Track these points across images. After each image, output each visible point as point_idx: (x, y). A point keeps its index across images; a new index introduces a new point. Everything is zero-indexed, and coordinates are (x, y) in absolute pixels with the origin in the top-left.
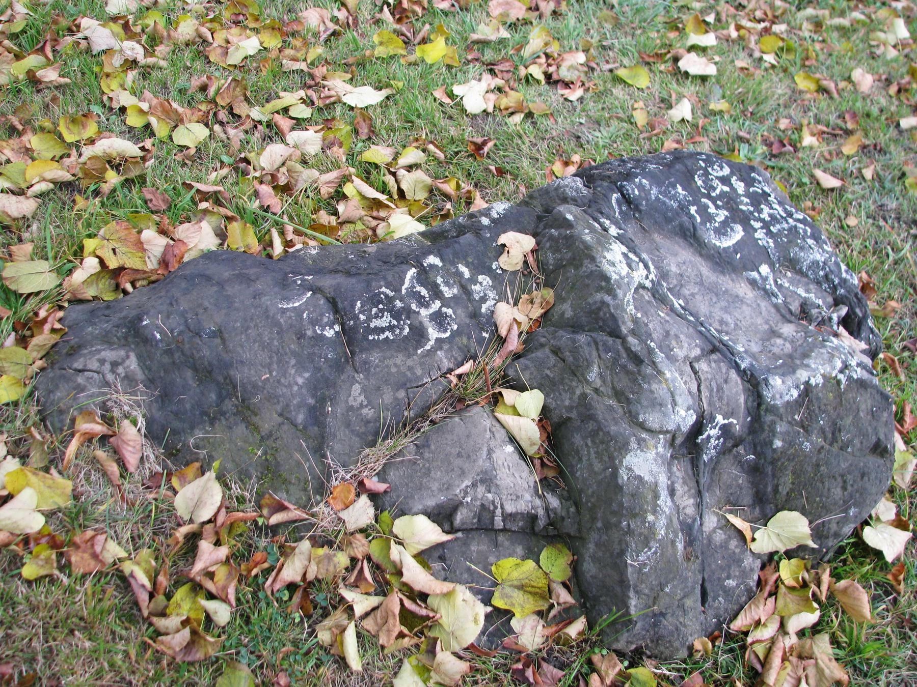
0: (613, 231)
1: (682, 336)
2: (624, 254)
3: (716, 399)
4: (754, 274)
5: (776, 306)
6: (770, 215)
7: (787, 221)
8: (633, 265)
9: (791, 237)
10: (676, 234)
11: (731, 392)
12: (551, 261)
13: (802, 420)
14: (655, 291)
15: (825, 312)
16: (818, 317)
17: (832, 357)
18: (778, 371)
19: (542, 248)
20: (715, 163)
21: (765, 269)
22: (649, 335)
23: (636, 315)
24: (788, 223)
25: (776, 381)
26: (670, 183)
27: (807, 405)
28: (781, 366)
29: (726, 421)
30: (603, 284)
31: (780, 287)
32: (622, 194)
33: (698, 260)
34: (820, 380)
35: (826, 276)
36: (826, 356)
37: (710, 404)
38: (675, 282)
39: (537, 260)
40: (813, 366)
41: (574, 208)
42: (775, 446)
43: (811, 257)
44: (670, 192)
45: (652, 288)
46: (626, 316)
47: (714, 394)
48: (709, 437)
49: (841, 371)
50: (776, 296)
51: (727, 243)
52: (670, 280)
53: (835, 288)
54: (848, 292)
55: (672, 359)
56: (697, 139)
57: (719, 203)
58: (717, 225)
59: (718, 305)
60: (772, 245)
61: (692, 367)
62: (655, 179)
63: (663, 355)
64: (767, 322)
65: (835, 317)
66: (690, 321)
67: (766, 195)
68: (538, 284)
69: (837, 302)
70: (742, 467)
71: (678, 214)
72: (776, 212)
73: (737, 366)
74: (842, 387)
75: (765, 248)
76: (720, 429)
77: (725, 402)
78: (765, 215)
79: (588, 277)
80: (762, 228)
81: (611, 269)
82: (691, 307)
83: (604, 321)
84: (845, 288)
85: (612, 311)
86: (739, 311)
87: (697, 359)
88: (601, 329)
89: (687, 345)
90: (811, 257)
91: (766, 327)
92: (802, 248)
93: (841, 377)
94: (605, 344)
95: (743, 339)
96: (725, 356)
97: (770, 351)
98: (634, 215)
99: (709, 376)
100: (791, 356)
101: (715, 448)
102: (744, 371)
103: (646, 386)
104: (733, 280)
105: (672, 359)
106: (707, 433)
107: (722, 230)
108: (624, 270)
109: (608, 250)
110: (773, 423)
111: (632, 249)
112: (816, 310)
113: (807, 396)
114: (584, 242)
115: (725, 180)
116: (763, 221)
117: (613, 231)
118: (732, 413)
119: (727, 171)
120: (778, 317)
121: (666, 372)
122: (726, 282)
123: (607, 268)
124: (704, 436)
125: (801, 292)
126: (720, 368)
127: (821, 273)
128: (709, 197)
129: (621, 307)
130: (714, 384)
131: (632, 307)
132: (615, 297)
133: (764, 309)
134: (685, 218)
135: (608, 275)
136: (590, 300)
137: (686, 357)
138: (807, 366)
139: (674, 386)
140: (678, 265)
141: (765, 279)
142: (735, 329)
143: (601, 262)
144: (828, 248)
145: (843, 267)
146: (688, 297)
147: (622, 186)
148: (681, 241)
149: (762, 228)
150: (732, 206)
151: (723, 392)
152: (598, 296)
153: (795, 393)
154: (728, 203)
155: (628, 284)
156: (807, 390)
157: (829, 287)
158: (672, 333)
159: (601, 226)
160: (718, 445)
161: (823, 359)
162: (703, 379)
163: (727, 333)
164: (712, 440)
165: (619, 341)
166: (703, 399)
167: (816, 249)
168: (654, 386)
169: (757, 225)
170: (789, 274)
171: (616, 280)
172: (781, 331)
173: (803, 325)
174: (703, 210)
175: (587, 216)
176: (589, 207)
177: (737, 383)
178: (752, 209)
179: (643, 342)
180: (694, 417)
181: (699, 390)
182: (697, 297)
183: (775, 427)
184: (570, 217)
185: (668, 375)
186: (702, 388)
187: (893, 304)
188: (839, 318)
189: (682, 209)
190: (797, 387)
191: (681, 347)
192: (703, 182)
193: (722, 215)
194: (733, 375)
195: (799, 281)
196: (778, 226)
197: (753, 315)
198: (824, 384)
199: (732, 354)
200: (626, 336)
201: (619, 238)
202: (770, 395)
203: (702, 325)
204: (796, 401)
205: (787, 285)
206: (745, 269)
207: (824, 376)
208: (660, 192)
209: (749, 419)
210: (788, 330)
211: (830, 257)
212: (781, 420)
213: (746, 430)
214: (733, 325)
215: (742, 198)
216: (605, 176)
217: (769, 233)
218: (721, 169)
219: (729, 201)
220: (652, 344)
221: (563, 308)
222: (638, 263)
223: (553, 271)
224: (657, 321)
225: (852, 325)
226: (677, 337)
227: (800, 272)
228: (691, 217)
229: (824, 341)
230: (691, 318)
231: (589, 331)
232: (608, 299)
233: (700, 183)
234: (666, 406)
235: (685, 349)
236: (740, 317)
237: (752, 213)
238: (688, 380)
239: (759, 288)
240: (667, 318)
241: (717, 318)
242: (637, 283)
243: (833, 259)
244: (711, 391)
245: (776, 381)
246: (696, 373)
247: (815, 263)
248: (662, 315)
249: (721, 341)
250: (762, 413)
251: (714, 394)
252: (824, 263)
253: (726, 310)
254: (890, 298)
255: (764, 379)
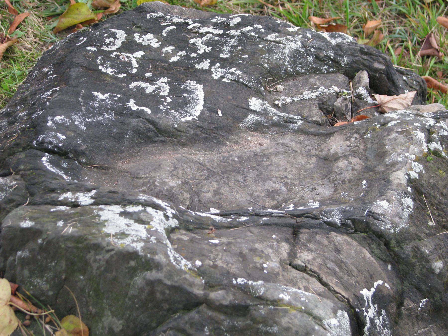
0: (85, 199)
1: (257, 245)
2: (121, 214)
3: (346, 277)
4: (251, 117)
5: (300, 131)
6: (207, 44)
7: (229, 35)
8: (143, 216)
9: (248, 48)
10: (139, 145)
11: (353, 257)
12: (45, 287)
13: (437, 222)
14: (186, 225)
15: (348, 94)
16: (346, 105)
17: (407, 133)
18: (373, 195)
19: (22, 281)
20: (101, 36)
21: (255, 103)
22: (229, 275)
23: (195, 266)
24: (232, 37)
25: (382, 206)
26: (83, 97)
27: (429, 202)
28: (369, 185)
29: (373, 290)
30: (133, 263)
31: (284, 108)
32: (50, 152)
33: (184, 152)
34: (419, 167)
35: (317, 57)
36: (402, 138)
37: (346, 288)
38: (187, 195)
39: (27, 299)
40: (400, 159)
41: (19, 211)
42: (437, 271)
43: (286, 51)
44: (94, 108)
45: (180, 224)
46: (187, 276)
47: (341, 274)
48: (372, 320)
49: (429, 140)
50: (292, 121)
51: (198, 109)
52: (181, 198)
53: (336, 62)
54: (352, 55)
55: (271, 277)
56: (19, 19)
57: (148, 75)
58: (169, 100)
59: (249, 181)
60: (239, 72)
61: (296, 267)
62: (69, 107)
63: (260, 282)
64: (310, 156)
65: (362, 90)
66: (245, 222)
67: (183, 26)
68: (50, 323)
69: (351, 74)
70: (423, 320)
71: (123, 123)
72: (210, 36)
73: (332, 226)
74: (443, 154)
75: (235, 81)
76: (374, 303)
77: (356, 273)
78: (203, 49)
79: (107, 270)
80: (212, 64)
81: (127, 241)
82: (228, 208)
83: (166, 301)
84: (345, 54)
85: (169, 283)
86: (273, 168)
87: (293, 255)
88: (172, 311)
89: (271, 251)
90: (286, 51)
91: (313, 160)
92: (270, 51)
93: (433, 146)
94: (192, 324)
95: (307, 194)
96: (311, 227)
97: (344, 182)
98: (80, 162)
99: (320, 261)
100: (368, 169)
101: (384, 326)
102: (343, 224)
103: (275, 329)
104: (236, 142)
105: (271, 277)
106: (368, 319)
107: (181, 102)
108: (141, 231)
109: (103, 224)
110: (416, 249)
111: (124, 201)
112: (340, 100)
113: (421, 193)
114: (70, 238)
115: (130, 46)
116: (205, 56)
117: (85, 199)
118: (371, 276)
119: (121, 35)
120: (314, 140)
121: (281, 296)
122: (231, 150)
123: (121, 243)
124: (368, 325)
125: (308, 95)
126: (319, 243)
127: (310, 59)
128: (134, 78)
129: (174, 272)
130: (331, 265)
131: (184, 262)
132: (158, 266)
133: (293, 144)
134: (135, 121)
135: (130, 250)
136: (132, 292)
137: (282, 262)
138: (394, 164)
139: (303, 303)
140: (173, 176)
141: (265, 113)
142: (290, 190)
143: (109, 244)
144: (293, 29)
145: (326, 35)
146: (215, 199)
147: (41, 143)
148: (150, 147)
149: (212, 64)
150: (163, 67)
151: (346, 264)
152: (139, 280)
153: (409, 202)
154: (155, 68)
155: (159, 241)
156: (417, 188)
157: (330, 66)
158: (246, 251)
159: (66, 205)
160: (384, 320)
161: (402, 144)
162: (316, 269)
163: (286, 201)
164: (377, 321)
165: (203, 308)
166: (337, 289)
167: (283, 39)
168: (284, 321)
169: (205, 65)
170: (280, 87)
171: (143, 249)
172: (332, 151)
173: (342, 128)
174: (141, 97)
175: (43, 207)
176: (32, 195)
177: (348, 243)
178: (184, 53)
179: (229, 287)
180: (346, 315)
181: (324, 284)
182: (222, 191)
183: (422, 253)
184: (27, 224)
185: (287, 298)
186: (324, 279)
187: (371, 24)
188: (366, 88)
189: (122, 114)
190: (405, 193)
191: (268, 258)
192: (112, 66)
193: (163, 85)
194: (339, 238)
195: (295, 86)
196: (226, 48)
197: (290, 159)
198: (425, 168)
199: (316, 218)
200: (206, 296)
201: (99, 201)
202: (389, 226)
203: (258, 215)
204: (416, 208)
205: (289, 100)
206: (238, 120)
207: (418, 160)
208: (85, 116)
209: (389, 267)
210: (336, 144)
211: (304, 36)
212: (420, 239)
213: (396, 281)
214: (283, 188)
215: (164, 50)
216: (10, 148)
217: (225, 63)
218: (115, 38)
219: (155, 64)
220: (240, 280)
221: (106, 324)
222: (145, 211)
223: (56, 296)
224: (219, 251)
225: (383, 84)
226: (253, 250)
227: (289, 76)
228: (138, 114)
229: (383, 125)
230: (244, 219)
231: (158, 324)
232: (152, 275)
233: (110, 71)
234: (314, 330)
235: (272, 256)
236: (282, 174)
237: (187, 57)
238: (305, 284)
239: (268, 128)
240: (224, 240)
241: (263, 195)
242: (164, 232)
243: (309, 35)
244: (335, 274)
245: (382, 206)
246: (304, 270)
247: (296, 54)
248: (216, 241)
249: (293, 215)
250: (397, 249)
251: (341, 274)
252: (304, 46)
253: (261, 179)
254: (364, 21)
255: (368, 215)
